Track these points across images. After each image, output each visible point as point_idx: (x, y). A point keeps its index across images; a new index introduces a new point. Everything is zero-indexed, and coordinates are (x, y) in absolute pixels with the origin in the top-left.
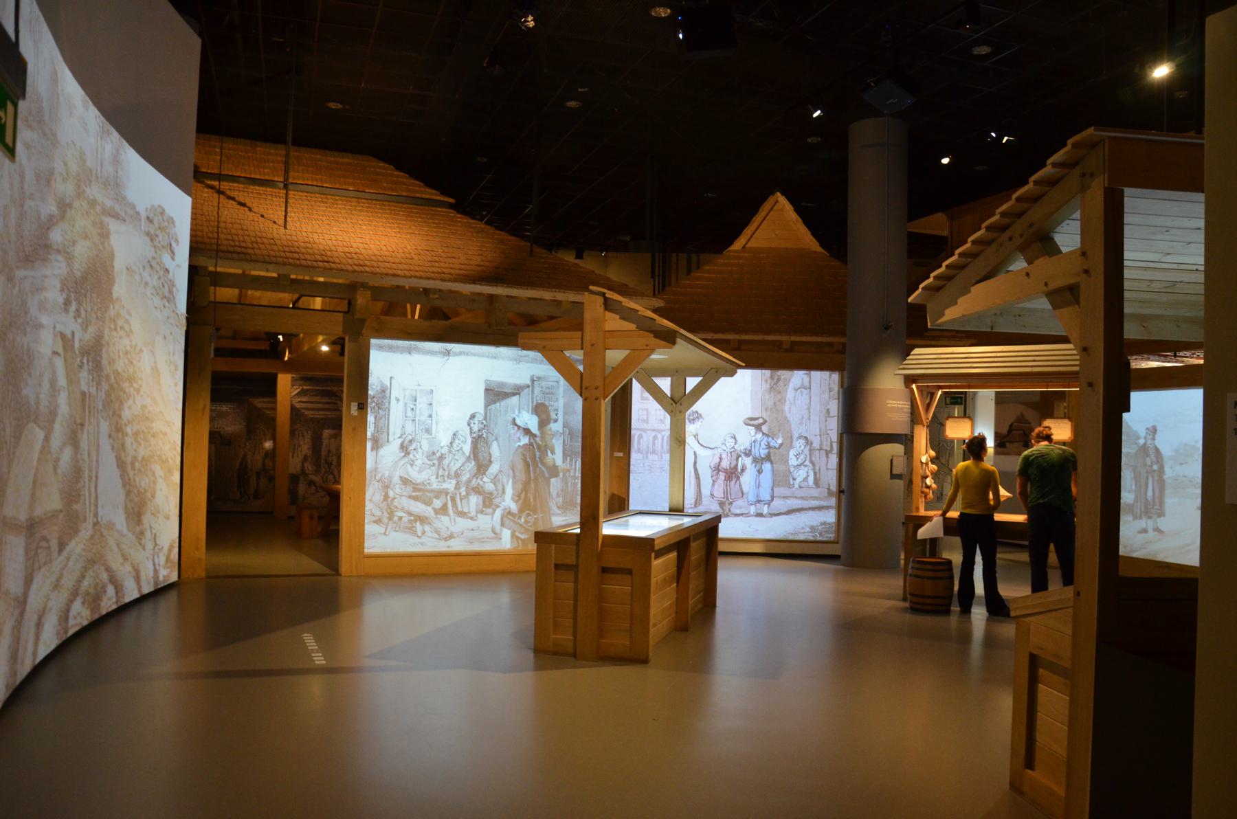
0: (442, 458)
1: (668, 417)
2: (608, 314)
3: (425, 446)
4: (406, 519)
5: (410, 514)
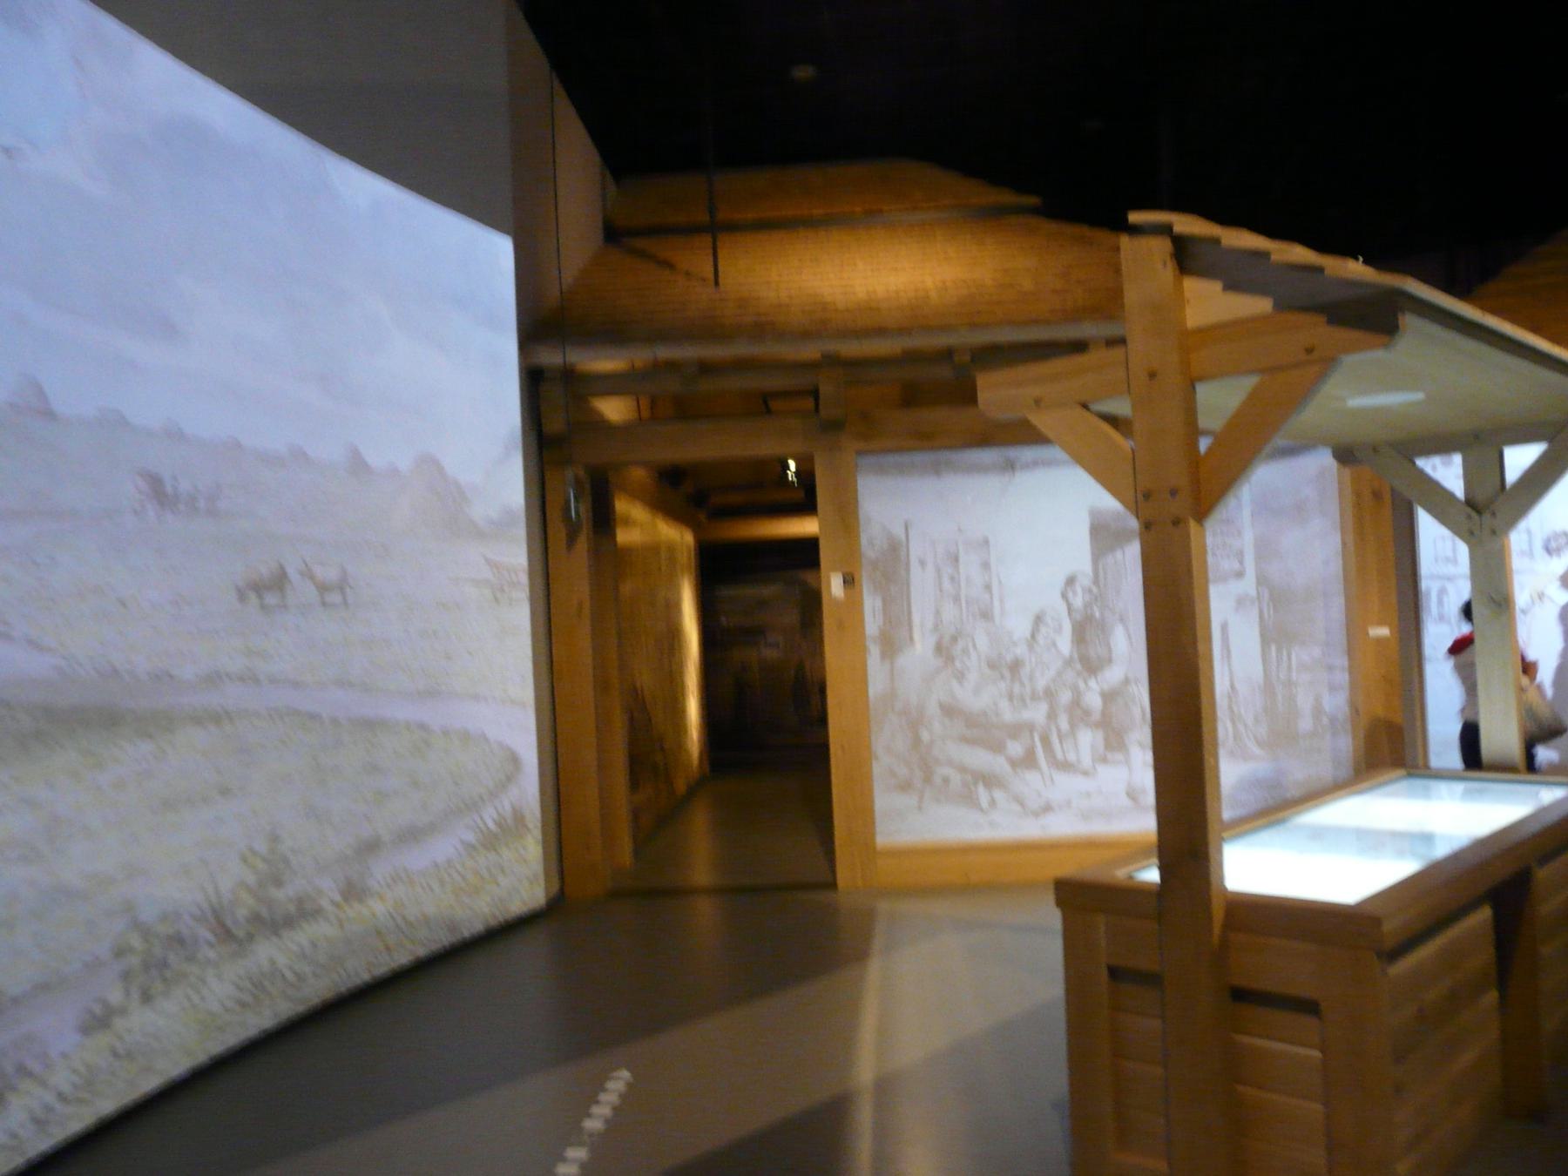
0: (1016, 666)
1: (1463, 550)
2: (1191, 285)
3: (982, 642)
4: (956, 778)
5: (962, 769)
